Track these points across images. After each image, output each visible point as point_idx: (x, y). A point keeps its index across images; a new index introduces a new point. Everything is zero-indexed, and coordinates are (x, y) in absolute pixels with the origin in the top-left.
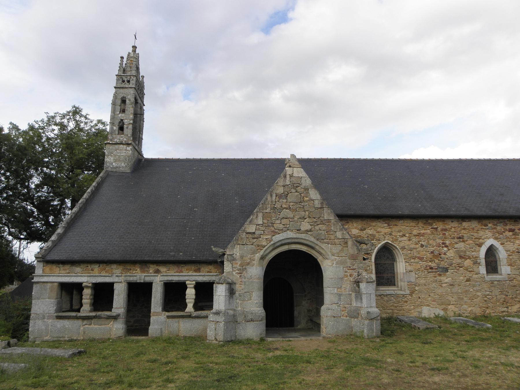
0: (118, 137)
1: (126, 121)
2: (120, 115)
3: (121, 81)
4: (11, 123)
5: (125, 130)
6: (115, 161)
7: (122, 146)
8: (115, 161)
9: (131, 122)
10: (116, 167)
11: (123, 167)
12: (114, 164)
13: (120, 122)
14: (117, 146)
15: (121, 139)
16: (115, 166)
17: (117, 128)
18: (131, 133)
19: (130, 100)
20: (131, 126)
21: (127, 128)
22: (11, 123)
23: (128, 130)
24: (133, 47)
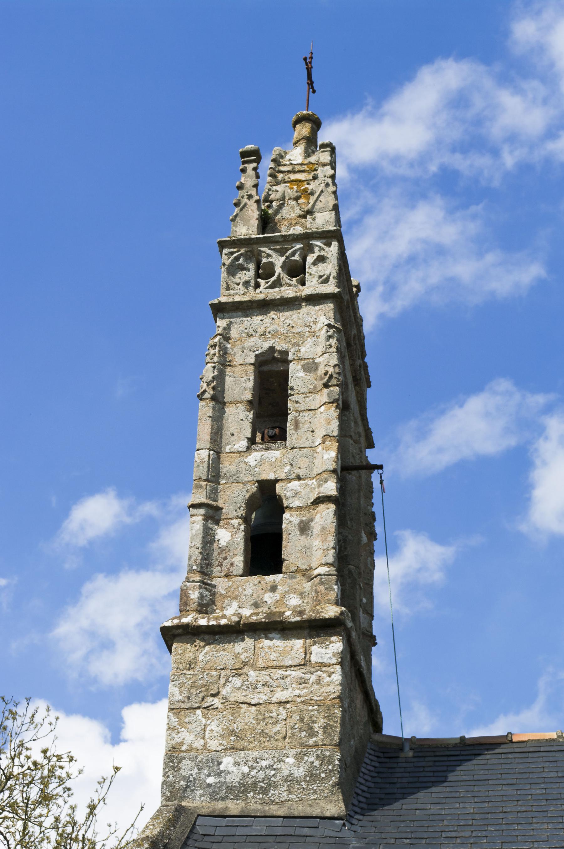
0: (252, 585)
1: (293, 493)
2: (253, 458)
3: (249, 274)
4: (76, 806)
5: (293, 548)
6: (236, 742)
7: (273, 647)
8: (236, 742)
9: (331, 487)
10: (243, 789)
11: (290, 780)
12: (227, 762)
13: (251, 504)
14: (243, 647)
15: (269, 598)
16: (234, 778)
17: (240, 537)
18: (331, 557)
19: (310, 366)
20: (326, 516)
21: (304, 528)
22: (76, 806)
23: (311, 544)
24: (89, 806)
